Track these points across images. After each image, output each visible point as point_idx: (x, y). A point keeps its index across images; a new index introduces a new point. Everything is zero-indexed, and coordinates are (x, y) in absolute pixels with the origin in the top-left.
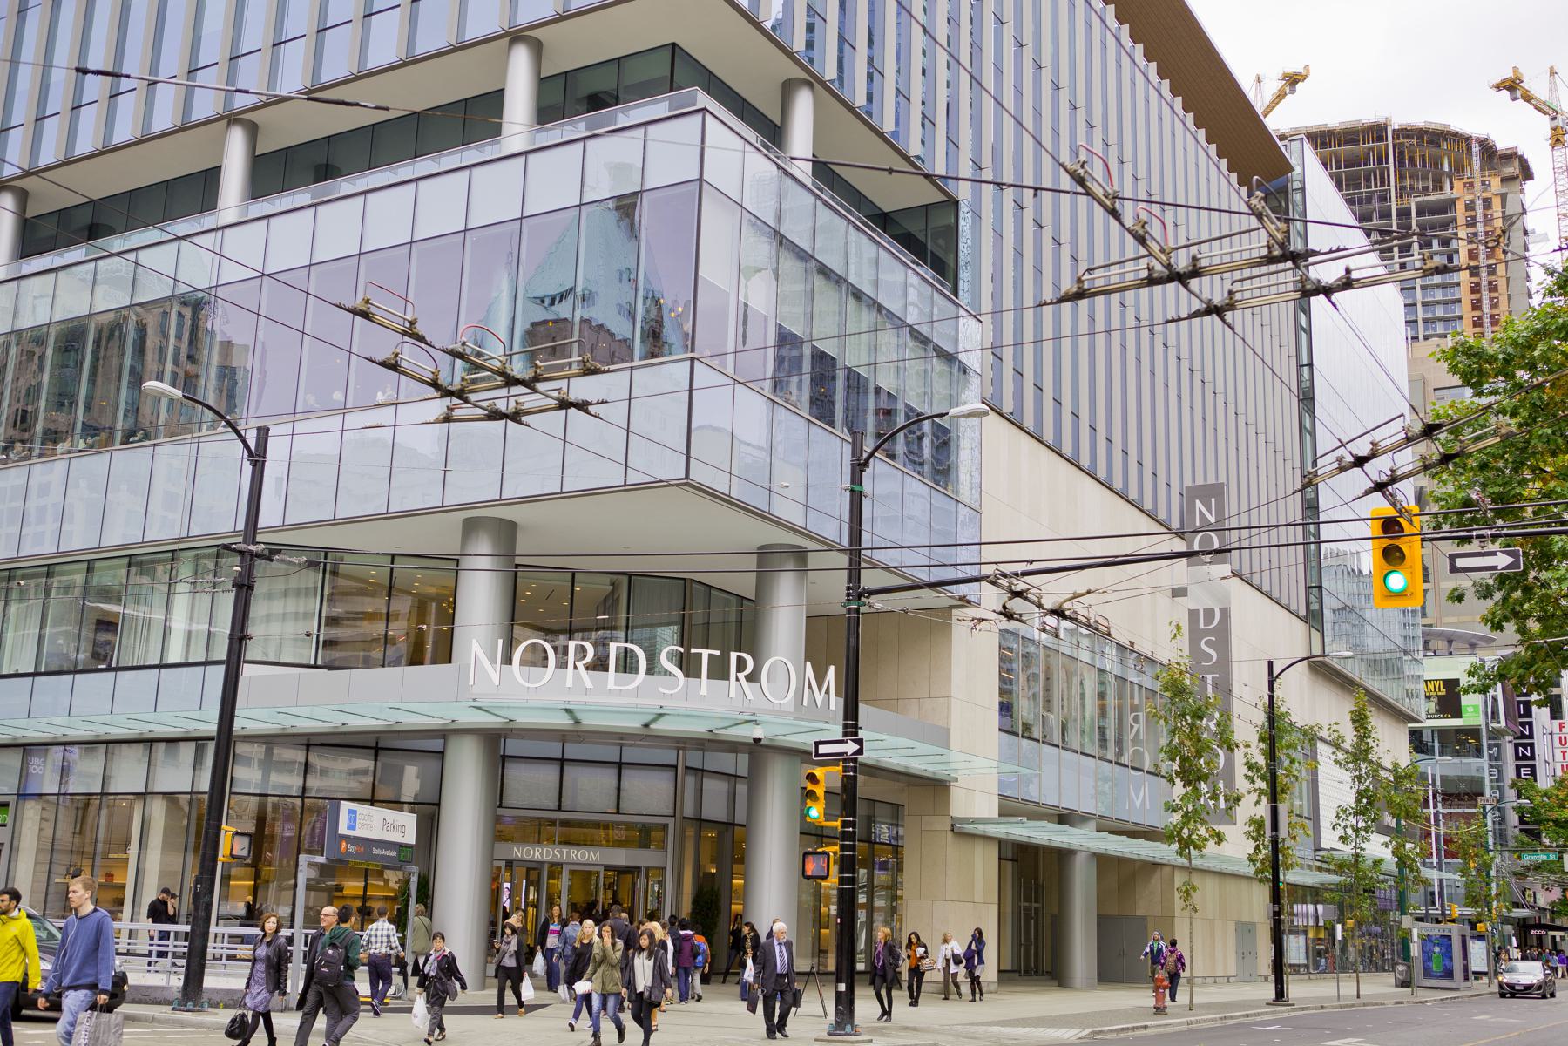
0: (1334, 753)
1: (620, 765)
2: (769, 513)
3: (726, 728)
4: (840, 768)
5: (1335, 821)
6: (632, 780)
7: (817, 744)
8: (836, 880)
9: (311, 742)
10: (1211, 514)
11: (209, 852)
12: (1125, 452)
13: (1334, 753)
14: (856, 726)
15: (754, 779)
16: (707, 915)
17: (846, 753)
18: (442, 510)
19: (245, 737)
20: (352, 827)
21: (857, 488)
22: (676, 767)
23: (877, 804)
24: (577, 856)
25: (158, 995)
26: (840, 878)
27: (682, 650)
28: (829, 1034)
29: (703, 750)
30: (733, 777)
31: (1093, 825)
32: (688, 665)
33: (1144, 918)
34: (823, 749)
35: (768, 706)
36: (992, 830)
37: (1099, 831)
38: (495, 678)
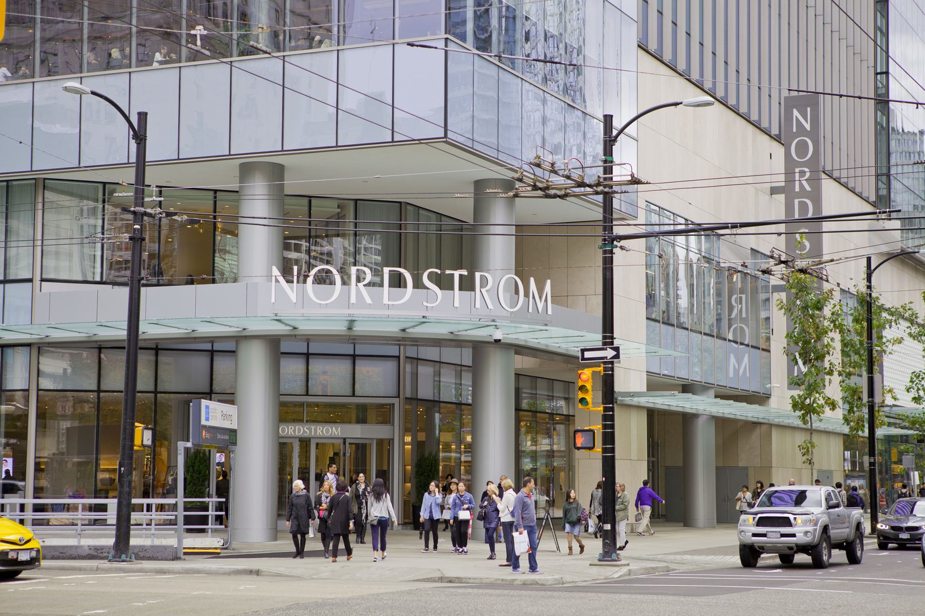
0: (908, 327)
1: (354, 357)
2: (498, 159)
3: (466, 330)
4: (601, 368)
5: (909, 384)
6: (363, 368)
7: (583, 351)
8: (600, 450)
9: (102, 346)
10: (807, 121)
11: (128, 443)
12: (660, 13)
13: (908, 327)
14: (612, 338)
15: (477, 369)
16: (429, 475)
17: (606, 357)
18: (230, 156)
19: (48, 343)
20: (207, 419)
21: (609, 158)
22: (398, 357)
23: (520, 377)
24: (322, 431)
25: (73, 552)
26: (603, 448)
27: (439, 272)
28: (600, 560)
29: (417, 345)
30: (459, 368)
31: (712, 393)
32: (444, 283)
33: (746, 468)
34: (587, 355)
35: (505, 314)
36: (643, 401)
37: (716, 397)
38: (293, 297)
